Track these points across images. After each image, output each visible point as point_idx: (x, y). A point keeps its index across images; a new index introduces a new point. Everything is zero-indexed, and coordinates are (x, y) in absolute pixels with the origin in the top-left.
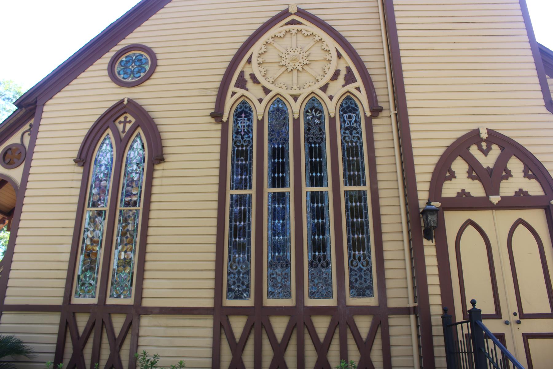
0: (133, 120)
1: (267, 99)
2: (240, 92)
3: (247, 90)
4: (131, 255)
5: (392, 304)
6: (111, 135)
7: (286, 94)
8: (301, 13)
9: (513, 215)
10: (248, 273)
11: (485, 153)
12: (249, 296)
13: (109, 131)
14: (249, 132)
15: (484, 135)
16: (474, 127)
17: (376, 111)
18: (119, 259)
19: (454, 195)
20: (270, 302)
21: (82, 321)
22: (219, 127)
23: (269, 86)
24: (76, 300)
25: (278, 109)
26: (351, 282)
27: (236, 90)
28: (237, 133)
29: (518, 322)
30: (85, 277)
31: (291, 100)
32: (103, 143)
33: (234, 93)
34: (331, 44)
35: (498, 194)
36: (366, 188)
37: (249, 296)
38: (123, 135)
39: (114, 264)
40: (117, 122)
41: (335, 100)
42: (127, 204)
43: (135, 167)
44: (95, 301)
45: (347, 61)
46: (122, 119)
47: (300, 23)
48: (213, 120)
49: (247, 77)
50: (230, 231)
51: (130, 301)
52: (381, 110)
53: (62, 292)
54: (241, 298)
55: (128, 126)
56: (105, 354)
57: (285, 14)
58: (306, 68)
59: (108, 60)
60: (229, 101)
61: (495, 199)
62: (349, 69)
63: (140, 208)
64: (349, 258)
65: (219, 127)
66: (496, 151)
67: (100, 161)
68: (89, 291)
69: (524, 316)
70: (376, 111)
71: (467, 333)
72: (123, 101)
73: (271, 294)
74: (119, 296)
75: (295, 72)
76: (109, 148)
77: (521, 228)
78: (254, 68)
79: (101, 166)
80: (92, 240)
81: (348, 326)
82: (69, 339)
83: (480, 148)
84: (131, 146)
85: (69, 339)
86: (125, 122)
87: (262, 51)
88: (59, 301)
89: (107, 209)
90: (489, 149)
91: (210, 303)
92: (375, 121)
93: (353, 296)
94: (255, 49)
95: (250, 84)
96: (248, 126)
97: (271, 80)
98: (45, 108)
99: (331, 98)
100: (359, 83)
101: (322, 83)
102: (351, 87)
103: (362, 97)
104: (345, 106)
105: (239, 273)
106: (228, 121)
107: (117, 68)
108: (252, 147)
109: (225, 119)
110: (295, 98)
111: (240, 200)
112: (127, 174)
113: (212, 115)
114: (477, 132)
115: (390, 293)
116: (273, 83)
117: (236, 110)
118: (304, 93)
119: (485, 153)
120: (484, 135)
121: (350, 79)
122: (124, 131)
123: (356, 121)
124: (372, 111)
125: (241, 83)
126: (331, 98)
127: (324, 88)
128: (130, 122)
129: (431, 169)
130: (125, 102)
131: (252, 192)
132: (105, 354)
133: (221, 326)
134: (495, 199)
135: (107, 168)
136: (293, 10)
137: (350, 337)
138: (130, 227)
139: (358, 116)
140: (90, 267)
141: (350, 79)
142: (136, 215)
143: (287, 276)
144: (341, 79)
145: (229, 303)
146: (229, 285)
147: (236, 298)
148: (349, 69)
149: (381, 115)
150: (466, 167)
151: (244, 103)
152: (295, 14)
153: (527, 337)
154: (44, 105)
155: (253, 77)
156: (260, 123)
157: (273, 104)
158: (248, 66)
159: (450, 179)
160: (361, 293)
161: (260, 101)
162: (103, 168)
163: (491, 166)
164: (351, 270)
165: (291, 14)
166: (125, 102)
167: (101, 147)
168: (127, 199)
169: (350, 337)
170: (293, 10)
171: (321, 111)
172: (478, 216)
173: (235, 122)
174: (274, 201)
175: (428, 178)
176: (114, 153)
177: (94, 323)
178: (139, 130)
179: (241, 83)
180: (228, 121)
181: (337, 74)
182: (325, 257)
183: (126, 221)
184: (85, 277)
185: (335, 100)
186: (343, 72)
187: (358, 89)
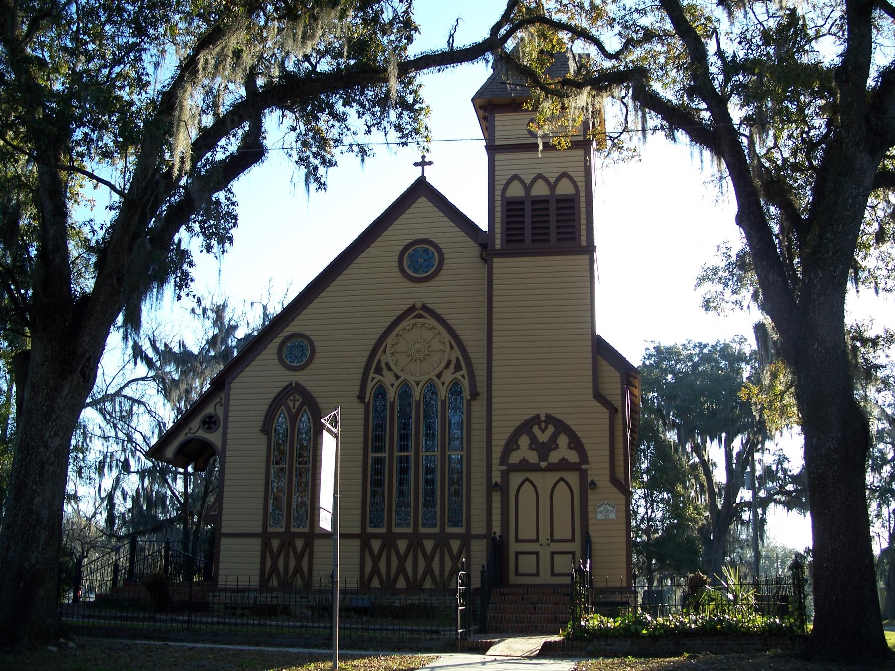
0: (301, 400)
1: (397, 384)
2: (378, 377)
3: (383, 376)
4: (306, 499)
5: (474, 532)
6: (285, 411)
7: (411, 379)
8: (424, 307)
9: (556, 476)
10: (383, 511)
11: (543, 431)
12: (383, 526)
13: (283, 407)
14: (384, 409)
15: (543, 418)
16: (537, 412)
17: (475, 395)
18: (297, 501)
20: (396, 530)
21: (276, 543)
22: (363, 406)
23: (399, 373)
24: (270, 530)
25: (405, 391)
26: (449, 518)
27: (376, 375)
31: (415, 385)
32: (279, 417)
33: (373, 379)
34: (447, 337)
35: (547, 460)
37: (383, 526)
38: (294, 411)
39: (294, 506)
40: (288, 400)
41: (446, 385)
42: (300, 463)
43: (304, 436)
44: (283, 530)
45: (457, 353)
46: (292, 398)
47: (424, 317)
48: (358, 400)
49: (383, 365)
50: (372, 455)
51: (306, 530)
52: (478, 394)
53: (260, 524)
54: (378, 527)
55: (297, 403)
56: (292, 564)
57: (413, 308)
58: (427, 358)
60: (370, 385)
61: (544, 464)
62: (458, 359)
63: (310, 466)
64: (449, 501)
65: (363, 406)
66: (551, 429)
67: (278, 431)
68: (279, 524)
69: (553, 540)
70: (475, 395)
73: (397, 525)
74: (299, 527)
75: (418, 361)
76: (284, 420)
77: (562, 483)
78: (388, 358)
79: (279, 434)
80: (278, 488)
82: (268, 555)
83: (540, 428)
84: (301, 419)
85: (268, 555)
86: (294, 400)
87: (394, 342)
88: (259, 530)
89: (287, 466)
90: (546, 428)
91: (358, 531)
92: (473, 403)
93: (449, 526)
94: (390, 340)
95: (385, 372)
96: (384, 405)
97: (401, 368)
98: (232, 386)
99: (443, 384)
100: (464, 372)
101: (437, 372)
102: (458, 375)
103: (466, 383)
104: (453, 389)
105: (377, 511)
106: (369, 402)
107: (285, 352)
108: (386, 422)
109: (367, 400)
110: (418, 384)
111: (378, 449)
112: (299, 441)
113: (358, 397)
114: (538, 416)
115: (473, 525)
116: (402, 370)
117: (375, 392)
118: (424, 379)
119: (543, 431)
120: (543, 418)
121: (458, 368)
122: (294, 408)
124: (471, 395)
125: (379, 371)
126: (443, 384)
127: (439, 376)
128: (298, 400)
130: (294, 385)
131: (386, 455)
132: (292, 564)
133: (266, 544)
134: (544, 464)
135: (284, 436)
136: (418, 305)
138: (304, 480)
139: (462, 398)
140: (278, 508)
141: (458, 368)
142: (307, 470)
143: (408, 514)
145: (370, 530)
146: (371, 519)
147: (375, 527)
149: (478, 398)
151: (381, 386)
152: (420, 309)
154: (231, 382)
155: (387, 364)
156: (392, 404)
157: (402, 387)
158: (383, 355)
159: (515, 450)
160: (456, 524)
161: (392, 385)
162: (281, 436)
163: (546, 441)
164: (449, 509)
165: (417, 309)
166: (294, 385)
167: (278, 419)
168: (300, 459)
170: (418, 305)
171: (436, 394)
172: (532, 476)
173: (375, 401)
174: (407, 445)
175: (501, 449)
176: (288, 424)
177: (284, 544)
178: (305, 407)
179: (379, 371)
180: (369, 402)
182: (433, 501)
183: (300, 475)
184: (275, 514)
185: (446, 385)
186: (454, 362)
187: (463, 376)
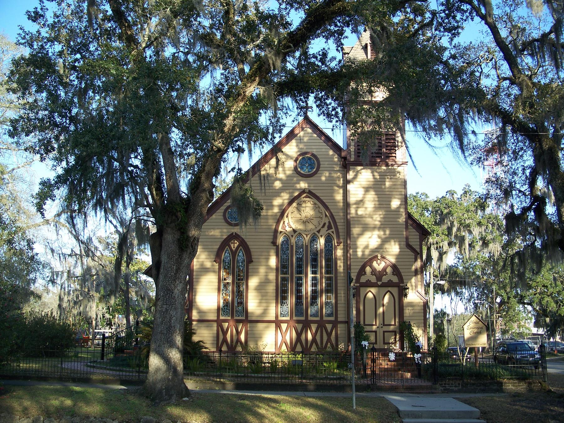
0: (238, 243)
13: (227, 247)
19: (365, 281)
28: (283, 250)
29: (382, 327)
30: (225, 309)
32: (225, 252)
36: (333, 276)
42: (239, 280)
43: (241, 264)
48: (272, 244)
59: (223, 211)
61: (379, 283)
69: (384, 325)
71: (365, 330)
72: (233, 233)
74: (239, 316)
81: (408, 312)
84: (238, 254)
86: (234, 243)
89: (231, 281)
96: (287, 247)
100: (333, 230)
101: (318, 229)
102: (330, 231)
112: (238, 267)
123: (331, 247)
129: (357, 271)
130: (234, 234)
134: (379, 283)
137: (324, 330)
144: (326, 226)
148: (329, 222)
150: (362, 277)
152: (307, 193)
153: (384, 332)
162: (227, 263)
169: (324, 330)
175: (356, 274)
176: (231, 257)
178: (241, 247)
181: (325, 224)
186: (327, 224)
187: (333, 232)
